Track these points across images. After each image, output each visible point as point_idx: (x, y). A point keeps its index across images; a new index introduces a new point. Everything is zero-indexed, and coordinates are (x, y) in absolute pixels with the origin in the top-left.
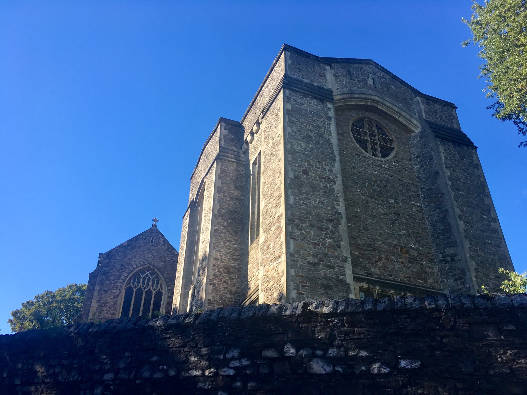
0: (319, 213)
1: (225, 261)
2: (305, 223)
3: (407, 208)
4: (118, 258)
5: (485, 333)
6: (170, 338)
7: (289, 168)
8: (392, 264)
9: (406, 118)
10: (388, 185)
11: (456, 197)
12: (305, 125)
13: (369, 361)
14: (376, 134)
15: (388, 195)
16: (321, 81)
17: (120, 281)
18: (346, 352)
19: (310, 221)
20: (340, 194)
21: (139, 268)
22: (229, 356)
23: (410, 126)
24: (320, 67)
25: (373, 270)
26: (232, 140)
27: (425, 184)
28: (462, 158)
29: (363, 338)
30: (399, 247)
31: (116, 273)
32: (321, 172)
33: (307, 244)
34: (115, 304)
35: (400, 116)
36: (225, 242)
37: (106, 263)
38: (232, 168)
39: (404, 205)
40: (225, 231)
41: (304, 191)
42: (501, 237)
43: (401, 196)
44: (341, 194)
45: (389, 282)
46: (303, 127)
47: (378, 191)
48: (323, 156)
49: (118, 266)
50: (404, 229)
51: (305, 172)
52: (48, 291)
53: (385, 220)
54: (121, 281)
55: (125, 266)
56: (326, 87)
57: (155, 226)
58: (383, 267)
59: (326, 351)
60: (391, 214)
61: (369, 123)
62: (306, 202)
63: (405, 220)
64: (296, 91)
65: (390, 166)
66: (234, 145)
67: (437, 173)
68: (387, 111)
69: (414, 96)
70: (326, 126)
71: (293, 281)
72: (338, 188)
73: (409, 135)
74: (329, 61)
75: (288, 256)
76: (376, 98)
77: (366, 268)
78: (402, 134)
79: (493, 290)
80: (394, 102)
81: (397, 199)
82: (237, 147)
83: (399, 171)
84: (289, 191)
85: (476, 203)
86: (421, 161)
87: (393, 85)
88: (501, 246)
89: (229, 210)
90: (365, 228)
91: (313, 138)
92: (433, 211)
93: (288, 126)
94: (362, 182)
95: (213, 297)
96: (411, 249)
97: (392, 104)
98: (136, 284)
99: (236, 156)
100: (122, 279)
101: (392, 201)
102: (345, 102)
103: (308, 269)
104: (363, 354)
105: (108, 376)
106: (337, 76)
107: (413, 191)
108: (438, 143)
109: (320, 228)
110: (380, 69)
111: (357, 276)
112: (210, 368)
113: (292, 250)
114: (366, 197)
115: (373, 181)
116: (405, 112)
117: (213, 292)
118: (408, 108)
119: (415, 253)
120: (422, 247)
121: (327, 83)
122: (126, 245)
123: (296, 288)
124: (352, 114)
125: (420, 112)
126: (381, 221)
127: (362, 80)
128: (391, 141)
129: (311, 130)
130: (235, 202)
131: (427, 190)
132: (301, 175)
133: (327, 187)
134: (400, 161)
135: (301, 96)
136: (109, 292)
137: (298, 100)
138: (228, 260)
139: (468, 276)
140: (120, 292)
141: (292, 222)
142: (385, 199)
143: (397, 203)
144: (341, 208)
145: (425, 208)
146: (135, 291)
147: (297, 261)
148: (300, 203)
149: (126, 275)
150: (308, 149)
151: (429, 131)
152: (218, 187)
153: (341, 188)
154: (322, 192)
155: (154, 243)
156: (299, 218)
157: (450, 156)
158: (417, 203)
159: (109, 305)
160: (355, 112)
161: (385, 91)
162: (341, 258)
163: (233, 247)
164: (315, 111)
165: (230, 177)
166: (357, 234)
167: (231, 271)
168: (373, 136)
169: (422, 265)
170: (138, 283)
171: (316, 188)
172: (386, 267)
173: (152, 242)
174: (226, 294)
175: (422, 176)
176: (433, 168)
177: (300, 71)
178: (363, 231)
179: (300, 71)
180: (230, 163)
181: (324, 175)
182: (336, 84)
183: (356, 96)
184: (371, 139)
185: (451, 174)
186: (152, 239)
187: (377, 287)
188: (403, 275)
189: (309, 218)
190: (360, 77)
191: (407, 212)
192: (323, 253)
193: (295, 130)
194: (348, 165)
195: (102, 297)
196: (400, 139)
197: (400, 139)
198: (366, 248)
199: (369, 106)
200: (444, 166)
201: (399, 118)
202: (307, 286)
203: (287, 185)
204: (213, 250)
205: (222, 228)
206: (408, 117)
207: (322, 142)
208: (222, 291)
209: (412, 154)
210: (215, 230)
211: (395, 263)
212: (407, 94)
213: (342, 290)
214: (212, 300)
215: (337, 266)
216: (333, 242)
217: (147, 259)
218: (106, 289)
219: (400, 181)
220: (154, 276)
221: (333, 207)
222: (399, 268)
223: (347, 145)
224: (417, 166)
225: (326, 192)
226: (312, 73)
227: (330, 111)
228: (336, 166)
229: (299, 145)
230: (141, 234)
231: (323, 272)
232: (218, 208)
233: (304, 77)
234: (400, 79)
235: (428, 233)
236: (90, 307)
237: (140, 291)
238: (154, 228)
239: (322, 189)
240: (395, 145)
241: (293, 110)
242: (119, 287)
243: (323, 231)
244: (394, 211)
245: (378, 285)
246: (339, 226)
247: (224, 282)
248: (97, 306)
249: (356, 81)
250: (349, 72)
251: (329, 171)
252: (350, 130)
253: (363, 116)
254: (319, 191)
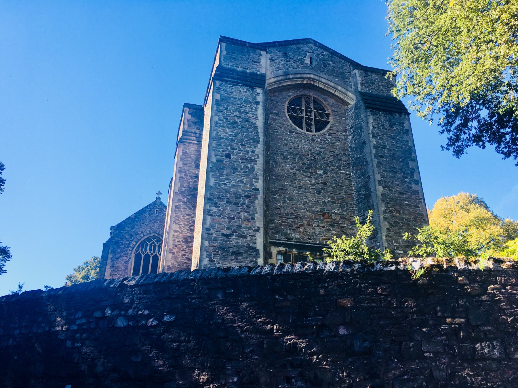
0: (237, 191)
1: (184, 233)
2: (223, 201)
3: (335, 177)
4: (127, 229)
5: (217, 295)
6: (49, 305)
7: (213, 153)
8: (313, 229)
9: (342, 92)
10: (318, 157)
11: (379, 164)
12: (232, 112)
13: (148, 317)
14: (313, 110)
15: (318, 167)
16: (255, 67)
17: (129, 249)
18: (138, 312)
19: (228, 199)
20: (260, 172)
21: (145, 237)
22: (76, 317)
23: (346, 99)
24: (256, 53)
25: (293, 235)
26: (195, 123)
27: (355, 153)
28: (391, 126)
29: (149, 302)
30: (322, 213)
31: (126, 243)
32: (243, 154)
33: (222, 219)
34: (126, 268)
35: (336, 91)
36: (184, 216)
37: (116, 234)
38: (193, 149)
39: (333, 175)
40: (185, 206)
41: (225, 173)
42: (421, 197)
43: (330, 166)
44: (261, 172)
45: (307, 244)
46: (231, 114)
47: (307, 164)
48: (247, 139)
49: (127, 237)
50: (329, 197)
51: (228, 156)
52: (94, 257)
53: (311, 190)
54: (130, 249)
55: (133, 236)
56: (259, 73)
57: (159, 198)
58: (303, 232)
59: (127, 311)
60: (318, 184)
61: (307, 100)
62: (226, 183)
63: (331, 189)
64: (226, 81)
65: (323, 139)
66: (197, 128)
67: (364, 142)
68: (323, 87)
69: (352, 68)
70: (254, 111)
71: (206, 251)
72: (258, 167)
73: (346, 107)
74: (264, 47)
75: (203, 230)
76: (312, 76)
77: (286, 234)
78: (340, 107)
79: (402, 246)
80: (330, 78)
81: (325, 170)
82: (199, 130)
83: (331, 143)
84: (211, 174)
85: (400, 168)
86: (354, 131)
87: (332, 61)
88: (419, 206)
89: (190, 188)
90: (291, 199)
91: (239, 124)
92: (359, 178)
93: (215, 115)
94: (292, 157)
95: (172, 264)
96: (333, 214)
97: (327, 80)
98: (144, 251)
99: (198, 138)
100: (131, 247)
101: (320, 172)
102: (280, 83)
103: (221, 240)
104: (146, 312)
105: (17, 332)
106: (273, 60)
107: (344, 161)
108: (369, 114)
109: (236, 204)
110: (319, 47)
111: (277, 241)
112: (66, 325)
113: (208, 225)
114: (295, 170)
115: (304, 155)
116: (340, 86)
117: (172, 259)
118: (345, 81)
119: (338, 218)
120: (346, 211)
121: (261, 68)
122: (134, 217)
123: (209, 256)
124: (290, 94)
125: (356, 85)
126: (307, 191)
127: (298, 60)
128: (328, 115)
129: (237, 116)
130: (195, 180)
131: (356, 159)
132: (223, 159)
133: (247, 167)
134: (333, 134)
135: (232, 86)
136: (121, 259)
137: (228, 89)
138: (187, 231)
139: (379, 235)
140: (130, 258)
141: (210, 201)
142: (313, 171)
143: (325, 173)
144: (260, 185)
145: (353, 175)
146: (143, 256)
147: (212, 234)
148: (220, 183)
149: (134, 244)
150: (233, 134)
151: (361, 103)
152: (179, 168)
153: (262, 167)
154: (243, 172)
155: (159, 214)
156: (217, 197)
157: (379, 125)
158: (346, 171)
159: (121, 270)
160: (293, 91)
161: (321, 68)
162: (253, 229)
163: (191, 220)
164: (244, 98)
165: (191, 158)
166: (281, 205)
167: (189, 240)
168: (309, 112)
169: (343, 227)
170: (146, 250)
171: (237, 169)
172: (307, 232)
173: (156, 213)
174: (184, 260)
175: (353, 146)
176: (362, 138)
177: (234, 61)
178: (288, 201)
179: (234, 61)
180: (192, 145)
181: (246, 156)
182: (271, 68)
183: (291, 76)
184: (306, 115)
185: (377, 142)
186: (157, 211)
187: (294, 250)
188: (323, 238)
189: (227, 196)
190: (297, 58)
191: (334, 180)
192: (237, 225)
193: (222, 118)
194: (281, 143)
195: (114, 264)
196: (337, 112)
197: (337, 112)
198: (289, 216)
199: (305, 84)
200: (371, 136)
201: (335, 92)
202: (219, 254)
203: (209, 169)
204: (173, 223)
205: (182, 204)
206: (344, 90)
207: (247, 126)
208: (180, 258)
209: (347, 125)
210: (176, 206)
211: (316, 228)
212: (345, 68)
213: (251, 256)
214: (171, 266)
215: (249, 235)
216: (247, 216)
217: (153, 228)
218: (117, 256)
219: (331, 153)
220: (159, 243)
221: (252, 184)
222: (319, 232)
223: (281, 123)
224: (351, 137)
225: (246, 172)
226: (247, 60)
227: (259, 95)
228: (259, 147)
229: (224, 132)
230: (147, 207)
231: (235, 241)
232: (179, 187)
233: (238, 66)
234: (339, 54)
235: (353, 198)
236: (105, 272)
237: (147, 257)
238: (158, 200)
239: (242, 169)
240: (331, 119)
241: (222, 100)
242: (129, 254)
243: (240, 206)
244: (322, 181)
245: (295, 248)
246: (255, 201)
247: (182, 250)
248: (111, 271)
249: (291, 62)
250: (286, 55)
251: (251, 152)
252: (286, 109)
253: (301, 94)
254: (239, 172)
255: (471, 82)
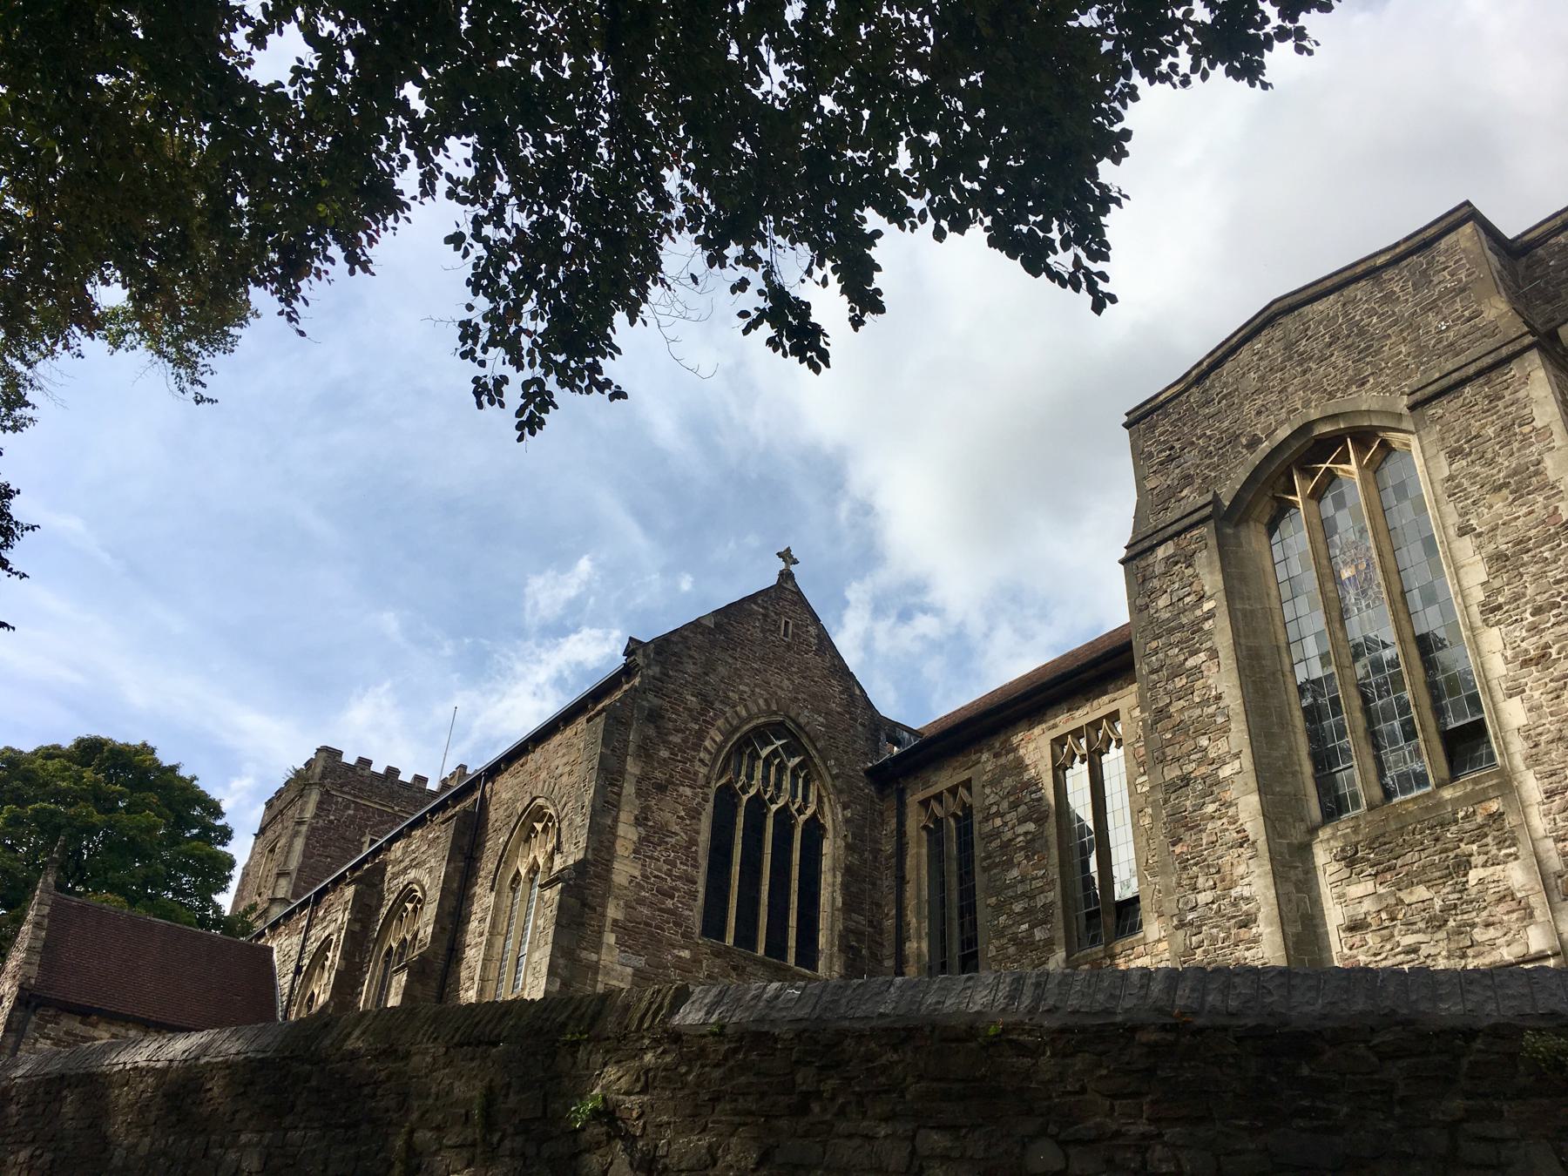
173: (786, 635)
255: (1358, 666)
